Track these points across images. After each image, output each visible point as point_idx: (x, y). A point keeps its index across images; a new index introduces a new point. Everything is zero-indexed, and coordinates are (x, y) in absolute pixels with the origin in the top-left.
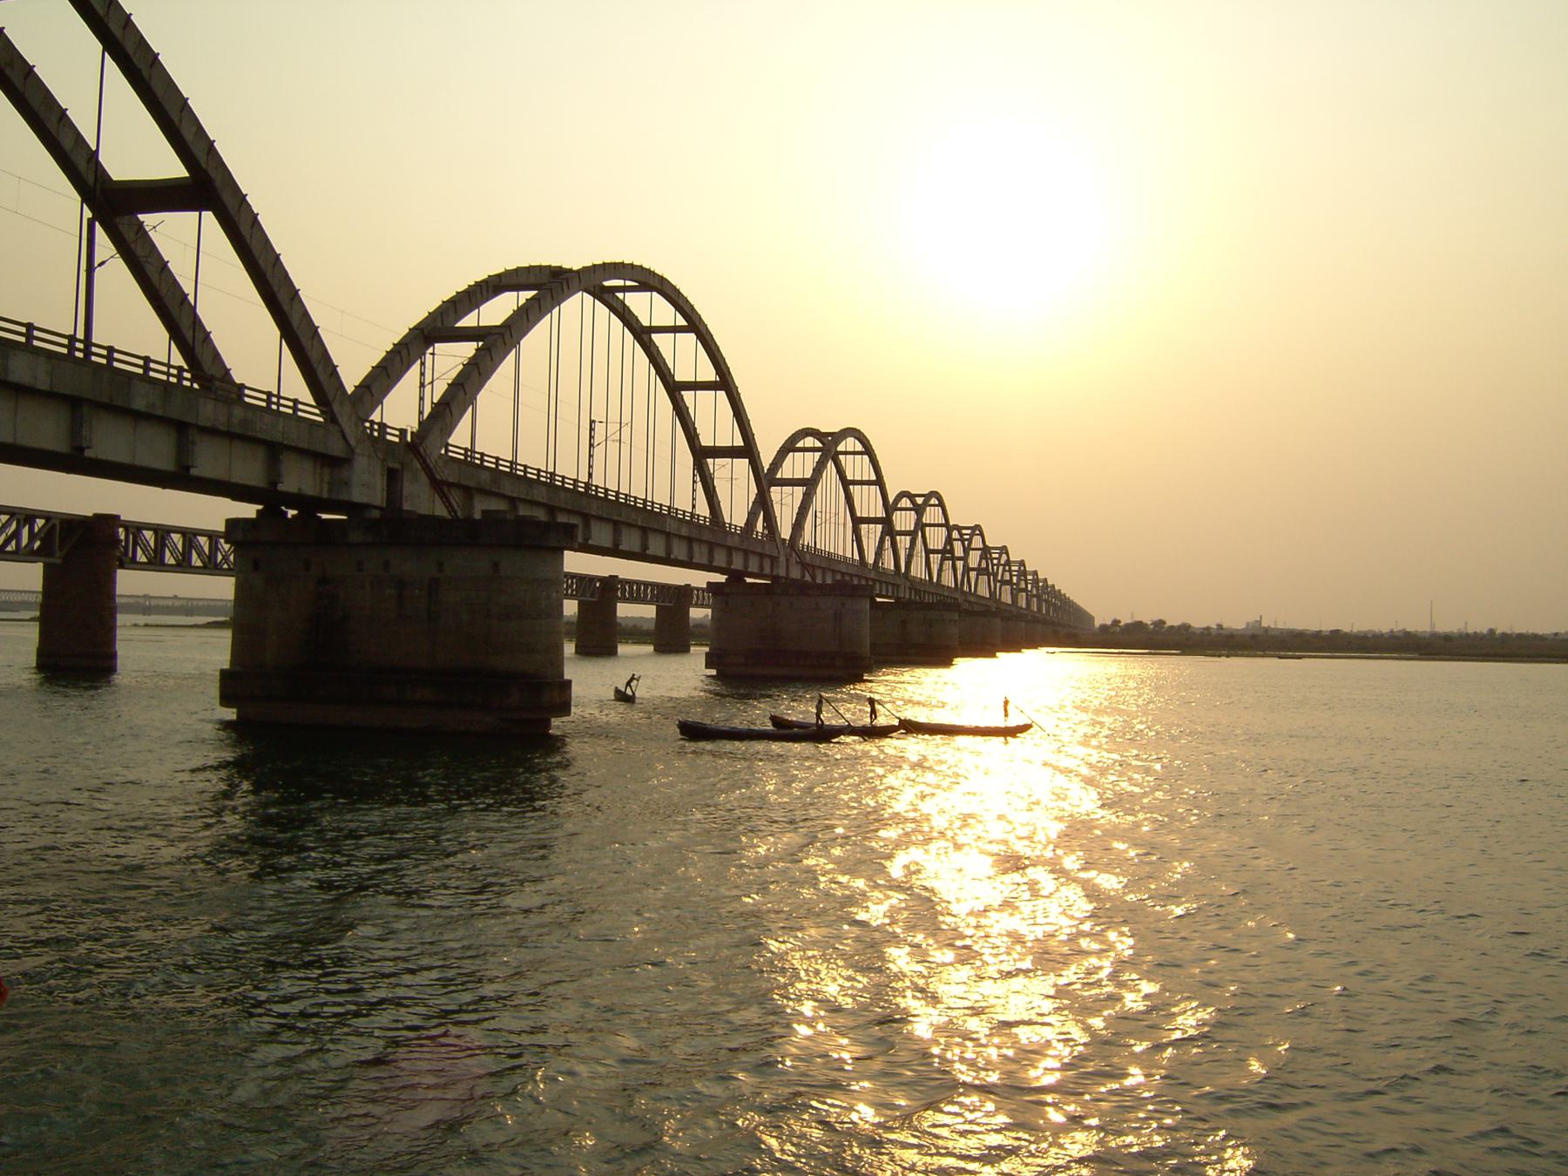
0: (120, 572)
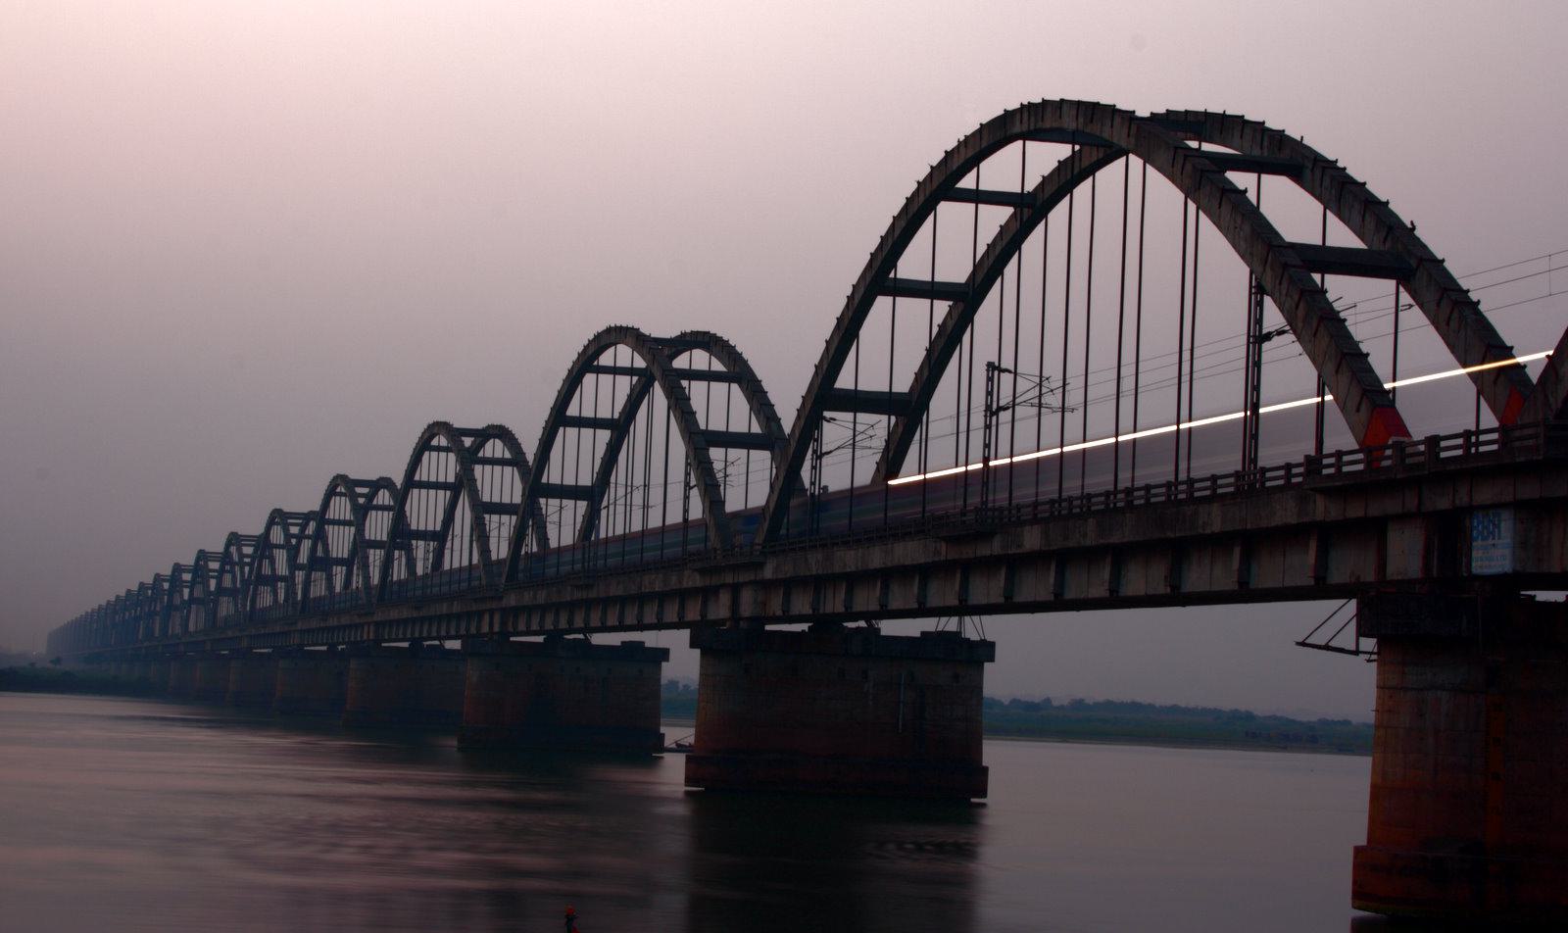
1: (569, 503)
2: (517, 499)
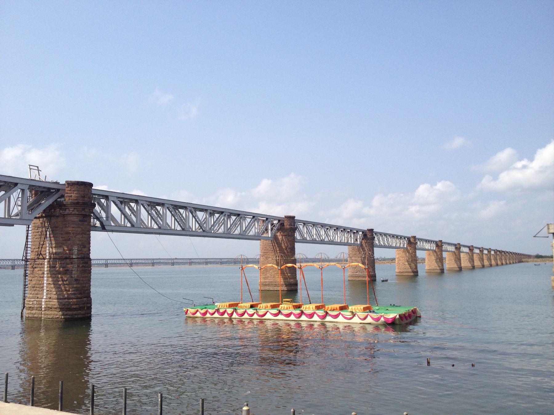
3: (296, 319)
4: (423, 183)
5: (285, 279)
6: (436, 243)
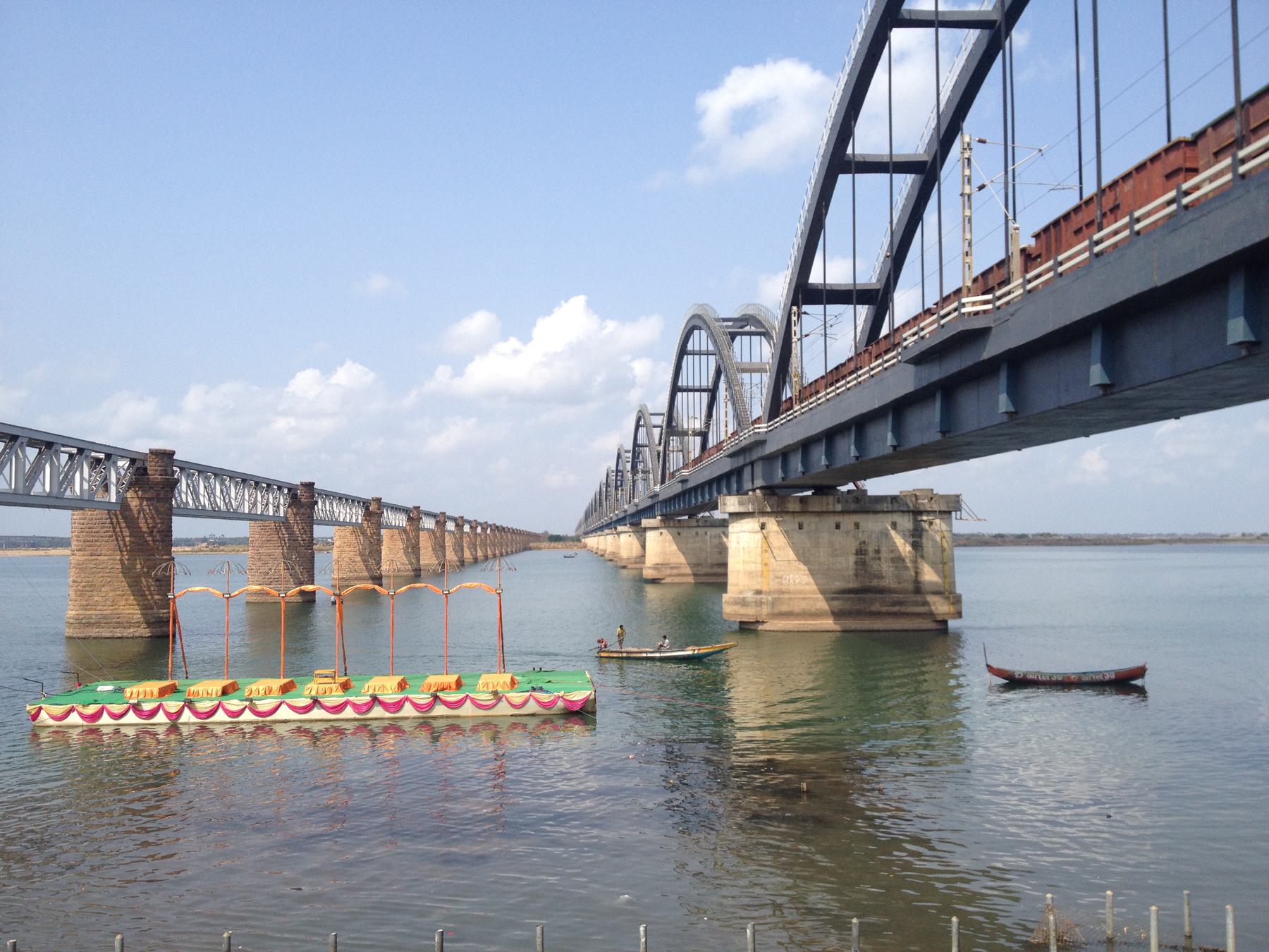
0: (174, 518)
1: (756, 376)
2: (679, 394)
3: (357, 716)
4: (303, 368)
5: (145, 607)
6: (365, 504)
